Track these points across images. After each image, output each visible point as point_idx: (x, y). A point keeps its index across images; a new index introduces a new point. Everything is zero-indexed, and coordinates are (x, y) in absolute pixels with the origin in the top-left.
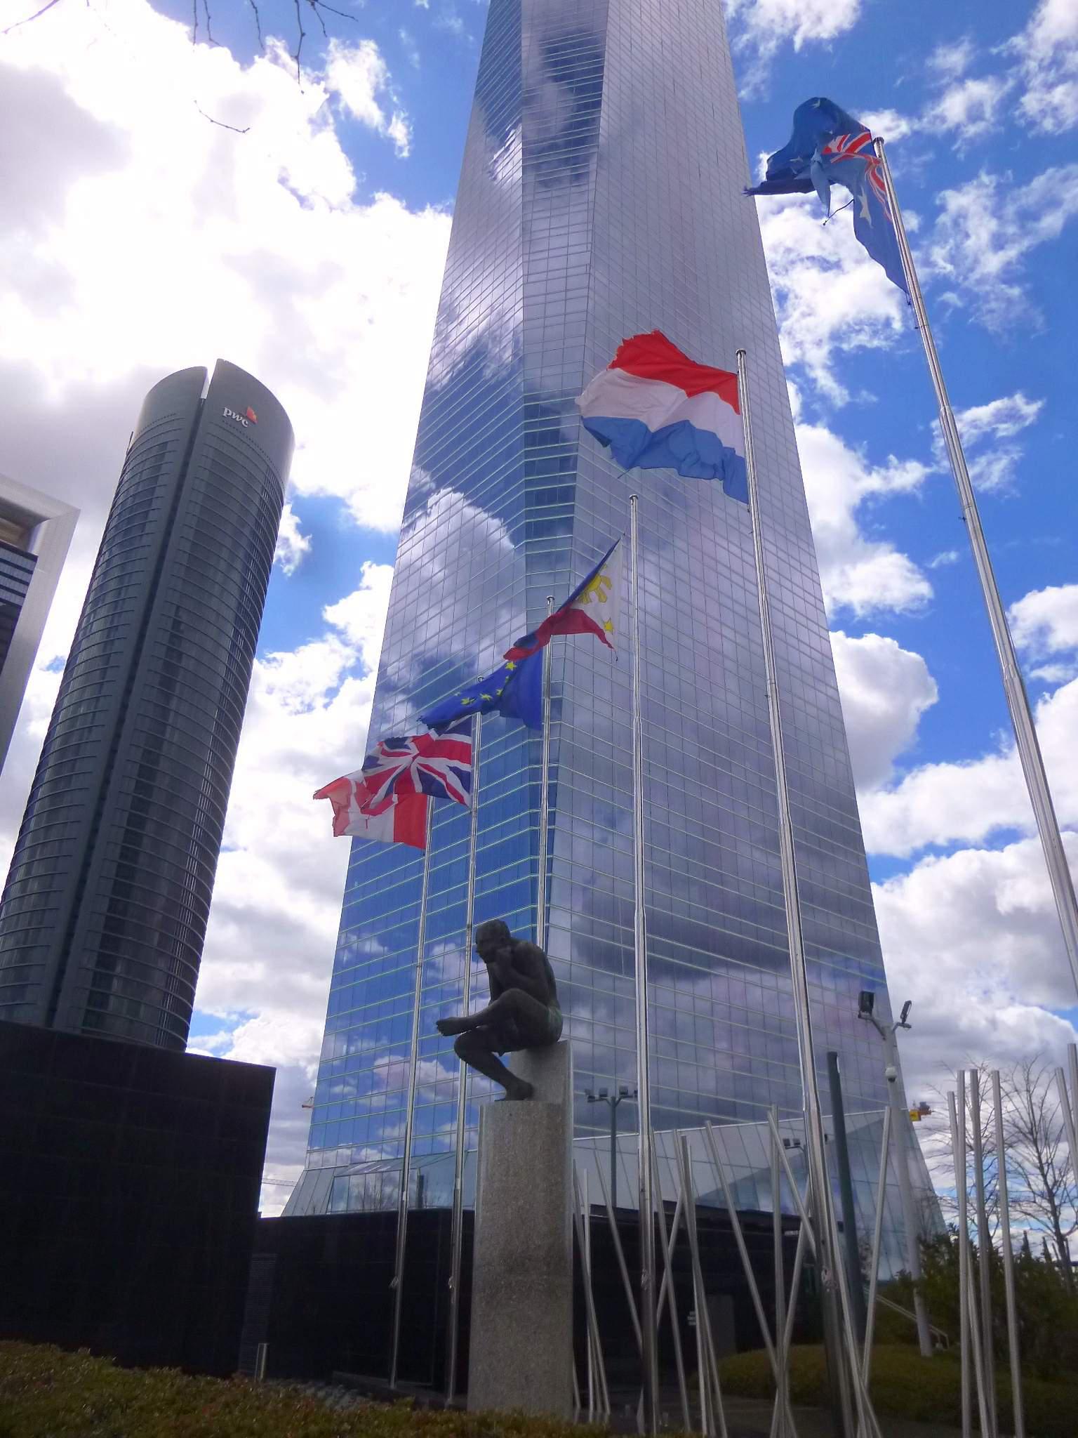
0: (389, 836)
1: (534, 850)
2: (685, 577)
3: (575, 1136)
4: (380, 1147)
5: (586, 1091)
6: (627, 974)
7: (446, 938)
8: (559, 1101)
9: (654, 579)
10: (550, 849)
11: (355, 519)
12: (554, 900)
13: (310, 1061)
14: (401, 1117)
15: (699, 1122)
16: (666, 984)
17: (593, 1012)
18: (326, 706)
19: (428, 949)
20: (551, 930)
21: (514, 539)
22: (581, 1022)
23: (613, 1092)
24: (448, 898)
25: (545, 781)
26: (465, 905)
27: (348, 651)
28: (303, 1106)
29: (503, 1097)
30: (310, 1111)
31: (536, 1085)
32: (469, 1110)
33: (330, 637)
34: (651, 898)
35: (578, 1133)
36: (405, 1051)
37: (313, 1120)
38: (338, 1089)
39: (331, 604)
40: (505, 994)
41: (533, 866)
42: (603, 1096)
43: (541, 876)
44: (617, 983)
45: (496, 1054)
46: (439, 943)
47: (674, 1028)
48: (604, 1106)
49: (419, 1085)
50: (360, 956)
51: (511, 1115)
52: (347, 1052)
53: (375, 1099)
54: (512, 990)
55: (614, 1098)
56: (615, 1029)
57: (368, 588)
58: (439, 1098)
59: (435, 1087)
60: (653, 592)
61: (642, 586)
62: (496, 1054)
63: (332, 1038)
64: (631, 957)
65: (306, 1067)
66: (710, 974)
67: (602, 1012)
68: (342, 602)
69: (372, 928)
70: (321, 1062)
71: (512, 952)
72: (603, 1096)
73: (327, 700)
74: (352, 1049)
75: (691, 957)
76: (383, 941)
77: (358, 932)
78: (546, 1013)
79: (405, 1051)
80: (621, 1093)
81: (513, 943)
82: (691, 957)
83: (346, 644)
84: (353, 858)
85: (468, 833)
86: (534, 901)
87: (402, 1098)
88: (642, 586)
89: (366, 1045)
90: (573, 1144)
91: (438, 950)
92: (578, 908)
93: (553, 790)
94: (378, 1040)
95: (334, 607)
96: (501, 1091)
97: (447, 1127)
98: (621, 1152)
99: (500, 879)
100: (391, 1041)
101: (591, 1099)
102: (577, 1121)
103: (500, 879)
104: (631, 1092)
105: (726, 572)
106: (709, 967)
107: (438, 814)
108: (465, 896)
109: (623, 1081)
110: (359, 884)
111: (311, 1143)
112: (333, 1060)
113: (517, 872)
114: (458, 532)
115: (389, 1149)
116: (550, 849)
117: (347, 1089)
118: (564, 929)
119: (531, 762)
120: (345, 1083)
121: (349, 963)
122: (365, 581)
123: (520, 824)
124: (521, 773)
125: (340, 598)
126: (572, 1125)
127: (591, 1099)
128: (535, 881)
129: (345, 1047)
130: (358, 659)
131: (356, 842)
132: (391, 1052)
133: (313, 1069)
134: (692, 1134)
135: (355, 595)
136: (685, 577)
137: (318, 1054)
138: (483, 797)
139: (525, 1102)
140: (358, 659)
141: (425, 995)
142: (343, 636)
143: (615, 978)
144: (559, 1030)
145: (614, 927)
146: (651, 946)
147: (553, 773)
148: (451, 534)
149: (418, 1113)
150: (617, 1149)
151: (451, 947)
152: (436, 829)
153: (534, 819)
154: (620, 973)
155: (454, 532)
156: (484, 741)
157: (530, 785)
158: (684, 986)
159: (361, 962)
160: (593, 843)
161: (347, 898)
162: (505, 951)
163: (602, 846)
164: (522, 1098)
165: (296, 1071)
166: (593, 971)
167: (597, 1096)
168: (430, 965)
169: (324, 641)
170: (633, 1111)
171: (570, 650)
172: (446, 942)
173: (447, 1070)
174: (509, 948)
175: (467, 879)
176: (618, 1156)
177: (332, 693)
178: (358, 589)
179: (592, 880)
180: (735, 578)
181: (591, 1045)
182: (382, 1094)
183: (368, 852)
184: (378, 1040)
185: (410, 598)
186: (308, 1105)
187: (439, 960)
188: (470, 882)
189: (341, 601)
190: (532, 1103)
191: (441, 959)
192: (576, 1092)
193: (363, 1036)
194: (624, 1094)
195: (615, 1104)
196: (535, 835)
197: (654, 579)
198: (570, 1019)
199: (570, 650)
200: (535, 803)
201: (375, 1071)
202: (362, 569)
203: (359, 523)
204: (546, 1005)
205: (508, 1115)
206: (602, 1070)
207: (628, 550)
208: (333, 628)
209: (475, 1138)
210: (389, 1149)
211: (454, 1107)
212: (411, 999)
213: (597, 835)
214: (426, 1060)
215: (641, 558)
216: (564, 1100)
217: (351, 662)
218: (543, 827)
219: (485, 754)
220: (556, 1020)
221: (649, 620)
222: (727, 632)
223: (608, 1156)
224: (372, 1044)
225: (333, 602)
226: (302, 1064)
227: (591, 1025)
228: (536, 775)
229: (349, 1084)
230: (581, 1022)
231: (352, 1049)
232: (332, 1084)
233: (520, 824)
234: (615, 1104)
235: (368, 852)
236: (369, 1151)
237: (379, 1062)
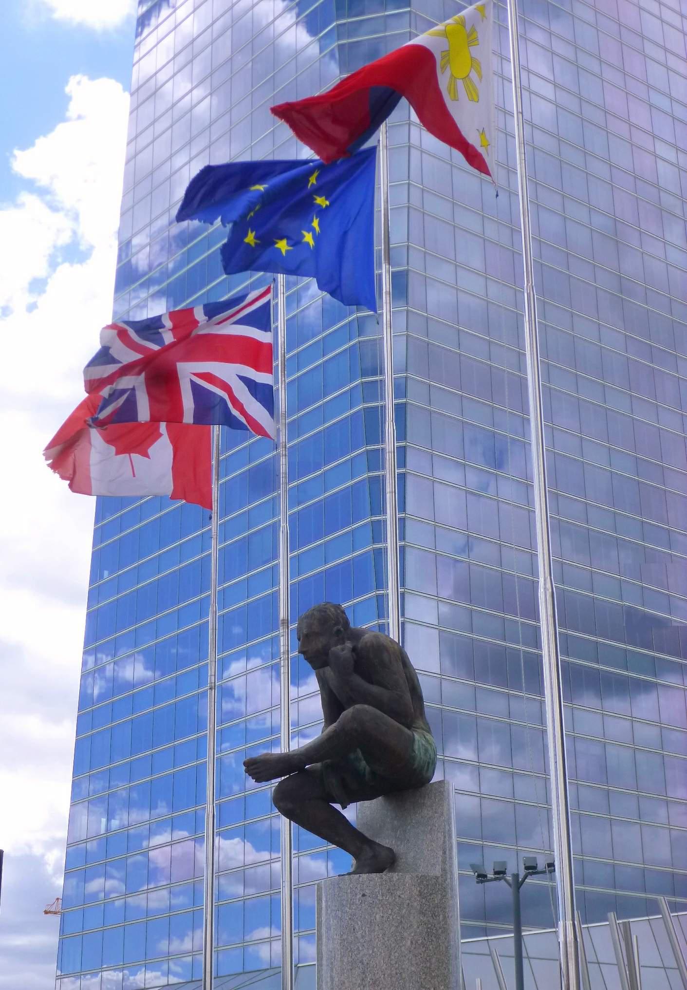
0: (167, 486)
1: (378, 507)
2: (594, 66)
3: (463, 937)
4: (165, 967)
5: (474, 867)
6: (528, 690)
7: (247, 649)
8: (437, 871)
9: (544, 70)
10: (402, 505)
11: (51, 10)
12: (411, 580)
13: (50, 845)
14: (195, 925)
15: (652, 908)
16: (589, 701)
17: (478, 750)
18: (32, 307)
19: (224, 665)
20: (408, 627)
21: (313, 25)
22: (461, 764)
23: (516, 867)
24: (249, 587)
25: (389, 402)
26: (275, 596)
27: (60, 220)
28: (46, 912)
29: (352, 870)
30: (57, 919)
31: (399, 848)
32: (297, 908)
33: (25, 197)
34: (560, 572)
35: (468, 932)
36: (195, 825)
37: (62, 931)
38: (95, 885)
39: (24, 147)
40: (347, 713)
41: (377, 532)
42: (500, 873)
43: (390, 544)
44: (514, 704)
45: (338, 806)
46: (237, 657)
47: (604, 771)
48: (501, 891)
49: (217, 873)
50: (116, 686)
51: (364, 895)
52: (107, 830)
53: (153, 896)
54: (358, 706)
55: (516, 876)
56: (513, 775)
57: (80, 117)
58: (251, 891)
59: (242, 874)
60: (542, 92)
61: (526, 85)
62: (338, 806)
63: (82, 810)
64: (535, 666)
65: (43, 856)
66: (655, 685)
67: (493, 751)
68: (41, 142)
69: (135, 639)
70: (69, 845)
71: (354, 650)
72: (500, 873)
73: (31, 299)
74: (115, 823)
75: (625, 660)
76: (154, 661)
77: (113, 648)
78: (412, 740)
79: (195, 825)
80: (527, 868)
81: (356, 635)
82: (625, 660)
83: (54, 208)
84: (100, 534)
85: (204, 586)
86: (381, 583)
87: (195, 894)
88: (526, 85)
89: (139, 816)
90: (461, 949)
91: (236, 667)
92: (446, 592)
93: (401, 411)
94: (152, 807)
95: (30, 152)
96: (349, 861)
97: (265, 932)
98: (529, 958)
99: (326, 554)
100: (173, 807)
101: (482, 877)
102: (464, 916)
103: (326, 554)
104: (541, 865)
105: (659, 54)
106: (655, 675)
107: (226, 459)
108: (275, 582)
109: (530, 849)
110: (110, 575)
111: (60, 967)
112: (86, 841)
113: (353, 541)
114: (228, 15)
115: (178, 969)
116: (402, 505)
117: (110, 883)
118: (429, 626)
119: (364, 374)
120: (107, 876)
121: (102, 697)
122: (73, 110)
123: (352, 468)
124: (351, 389)
125: (37, 137)
126: (457, 923)
127: (482, 877)
128: (380, 554)
129: (104, 820)
130: (75, 233)
131: (104, 507)
132: (173, 825)
133: (56, 857)
134: (639, 925)
135: (61, 127)
136: (594, 66)
137: (63, 834)
138: (295, 429)
139: (385, 875)
140: (75, 233)
141: (222, 736)
142: (48, 197)
143: (508, 696)
144: (431, 765)
145: (504, 619)
146: (565, 645)
147: (400, 390)
148: (218, 19)
149: (219, 914)
150: (524, 954)
151: (256, 662)
152: (223, 483)
153: (375, 460)
154: (520, 689)
155: (222, 16)
156: (290, 347)
157: (364, 409)
158: (616, 704)
159: (120, 693)
160: (466, 492)
161: (94, 595)
162: (343, 650)
163: (480, 496)
164: (380, 871)
165: (32, 862)
166: (475, 688)
167: (491, 876)
168: (226, 693)
169: (17, 206)
170: (548, 898)
171: (415, 194)
172: (248, 655)
173: (258, 848)
174: (349, 645)
175: (275, 556)
176: (525, 962)
177: (38, 286)
178: (64, 119)
179: (467, 547)
180: (609, 74)
181: (477, 800)
182: (162, 888)
183: (121, 523)
184: (152, 807)
185: (160, 126)
186: (53, 909)
187: (238, 686)
188: (282, 561)
189: (37, 141)
190: (395, 876)
191: (242, 680)
192: (459, 839)
193: (129, 805)
194: (532, 869)
195: (518, 884)
196: (377, 484)
197: (544, 70)
198: (444, 761)
199: (415, 194)
200: (374, 433)
201: (151, 854)
202: (67, 89)
203: (57, 16)
204: (409, 728)
205: (359, 896)
206: (496, 838)
207: (502, 28)
208: (30, 185)
209: (310, 950)
210: (178, 969)
211: (274, 904)
212: (200, 743)
213: (473, 479)
214: (227, 835)
215: (522, 38)
216: (444, 870)
217: (65, 238)
218: (389, 472)
219: (297, 362)
220: (426, 750)
221: (539, 138)
222: (663, 150)
223: (512, 962)
224: (146, 816)
225: (26, 144)
226: (37, 851)
227: (478, 769)
228: (374, 390)
229: (112, 877)
230: (461, 764)
231: (115, 823)
232: (86, 877)
233: (352, 468)
234: (518, 884)
235: (121, 523)
236: (150, 975)
237: (157, 840)
